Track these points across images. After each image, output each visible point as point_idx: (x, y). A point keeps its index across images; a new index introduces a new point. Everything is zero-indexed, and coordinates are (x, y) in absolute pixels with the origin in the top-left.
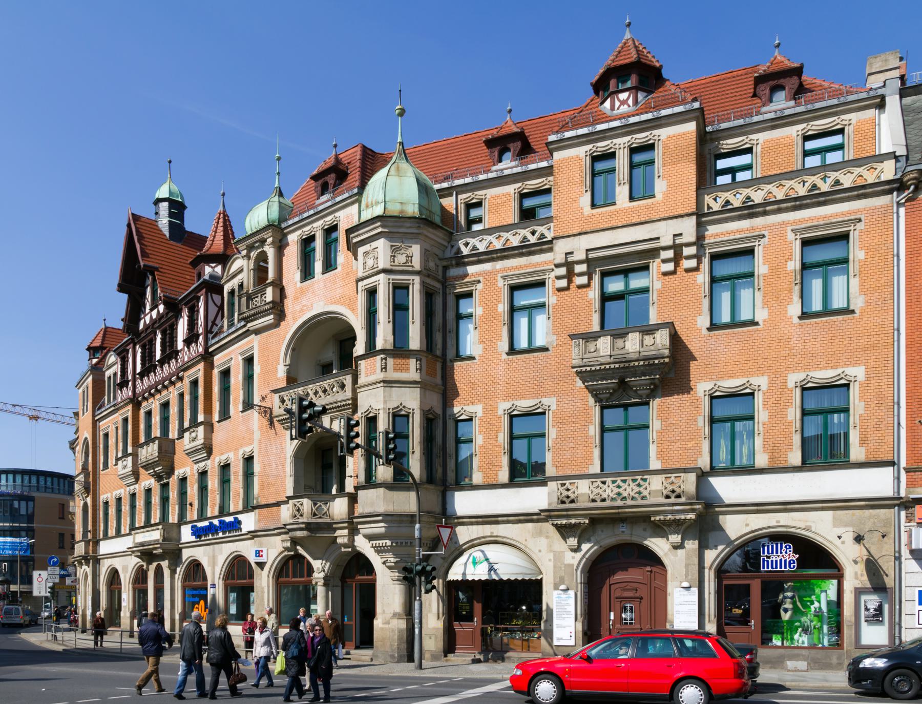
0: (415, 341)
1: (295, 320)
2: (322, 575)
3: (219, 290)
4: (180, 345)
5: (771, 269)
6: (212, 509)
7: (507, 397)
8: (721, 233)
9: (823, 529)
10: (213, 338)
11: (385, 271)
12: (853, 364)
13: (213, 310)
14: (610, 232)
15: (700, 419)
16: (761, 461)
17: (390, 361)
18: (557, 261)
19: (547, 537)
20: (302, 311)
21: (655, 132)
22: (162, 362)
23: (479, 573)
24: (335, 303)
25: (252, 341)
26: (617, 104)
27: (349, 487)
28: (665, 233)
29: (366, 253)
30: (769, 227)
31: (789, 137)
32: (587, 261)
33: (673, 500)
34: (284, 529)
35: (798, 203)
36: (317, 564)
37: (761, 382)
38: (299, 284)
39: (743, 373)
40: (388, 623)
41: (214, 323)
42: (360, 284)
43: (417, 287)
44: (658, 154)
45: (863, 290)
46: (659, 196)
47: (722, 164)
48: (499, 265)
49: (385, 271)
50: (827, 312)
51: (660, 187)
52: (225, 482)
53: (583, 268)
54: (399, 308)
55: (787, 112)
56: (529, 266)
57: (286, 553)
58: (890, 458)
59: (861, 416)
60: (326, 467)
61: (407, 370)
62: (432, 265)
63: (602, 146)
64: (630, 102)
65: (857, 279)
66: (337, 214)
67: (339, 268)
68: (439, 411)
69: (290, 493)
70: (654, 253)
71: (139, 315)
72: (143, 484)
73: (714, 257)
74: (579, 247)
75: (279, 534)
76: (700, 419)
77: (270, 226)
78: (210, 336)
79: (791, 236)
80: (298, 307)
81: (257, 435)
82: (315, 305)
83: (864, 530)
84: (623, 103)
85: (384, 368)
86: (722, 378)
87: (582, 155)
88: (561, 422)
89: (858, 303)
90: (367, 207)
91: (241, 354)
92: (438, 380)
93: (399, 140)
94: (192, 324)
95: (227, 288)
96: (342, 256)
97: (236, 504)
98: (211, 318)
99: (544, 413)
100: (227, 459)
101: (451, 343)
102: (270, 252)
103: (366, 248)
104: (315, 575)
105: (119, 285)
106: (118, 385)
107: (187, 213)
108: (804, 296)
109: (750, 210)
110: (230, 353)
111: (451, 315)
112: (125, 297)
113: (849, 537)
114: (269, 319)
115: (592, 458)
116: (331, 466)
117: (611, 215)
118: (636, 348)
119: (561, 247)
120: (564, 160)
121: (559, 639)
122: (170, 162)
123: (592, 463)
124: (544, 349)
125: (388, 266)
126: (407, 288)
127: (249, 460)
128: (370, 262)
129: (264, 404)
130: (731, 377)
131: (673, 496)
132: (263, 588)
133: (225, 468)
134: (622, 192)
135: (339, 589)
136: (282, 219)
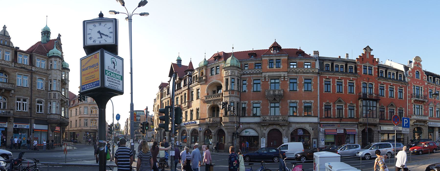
3: (191, 76)
4: (182, 86)
6: (189, 119)
9: (308, 127)
13: (189, 80)
16: (298, 115)
22: (177, 90)
23: (247, 134)
28: (282, 74)
34: (207, 124)
36: (212, 131)
44: (281, 61)
47: (291, 64)
51: (281, 66)
52: (192, 114)
60: (214, 111)
63: (271, 58)
85: (229, 94)
89: (313, 90)
94: (185, 83)
95: (193, 76)
97: (194, 117)
111: (242, 84)
113: (311, 129)
114: (204, 82)
119: (263, 74)
124: (259, 91)
127: (198, 110)
133: (192, 111)
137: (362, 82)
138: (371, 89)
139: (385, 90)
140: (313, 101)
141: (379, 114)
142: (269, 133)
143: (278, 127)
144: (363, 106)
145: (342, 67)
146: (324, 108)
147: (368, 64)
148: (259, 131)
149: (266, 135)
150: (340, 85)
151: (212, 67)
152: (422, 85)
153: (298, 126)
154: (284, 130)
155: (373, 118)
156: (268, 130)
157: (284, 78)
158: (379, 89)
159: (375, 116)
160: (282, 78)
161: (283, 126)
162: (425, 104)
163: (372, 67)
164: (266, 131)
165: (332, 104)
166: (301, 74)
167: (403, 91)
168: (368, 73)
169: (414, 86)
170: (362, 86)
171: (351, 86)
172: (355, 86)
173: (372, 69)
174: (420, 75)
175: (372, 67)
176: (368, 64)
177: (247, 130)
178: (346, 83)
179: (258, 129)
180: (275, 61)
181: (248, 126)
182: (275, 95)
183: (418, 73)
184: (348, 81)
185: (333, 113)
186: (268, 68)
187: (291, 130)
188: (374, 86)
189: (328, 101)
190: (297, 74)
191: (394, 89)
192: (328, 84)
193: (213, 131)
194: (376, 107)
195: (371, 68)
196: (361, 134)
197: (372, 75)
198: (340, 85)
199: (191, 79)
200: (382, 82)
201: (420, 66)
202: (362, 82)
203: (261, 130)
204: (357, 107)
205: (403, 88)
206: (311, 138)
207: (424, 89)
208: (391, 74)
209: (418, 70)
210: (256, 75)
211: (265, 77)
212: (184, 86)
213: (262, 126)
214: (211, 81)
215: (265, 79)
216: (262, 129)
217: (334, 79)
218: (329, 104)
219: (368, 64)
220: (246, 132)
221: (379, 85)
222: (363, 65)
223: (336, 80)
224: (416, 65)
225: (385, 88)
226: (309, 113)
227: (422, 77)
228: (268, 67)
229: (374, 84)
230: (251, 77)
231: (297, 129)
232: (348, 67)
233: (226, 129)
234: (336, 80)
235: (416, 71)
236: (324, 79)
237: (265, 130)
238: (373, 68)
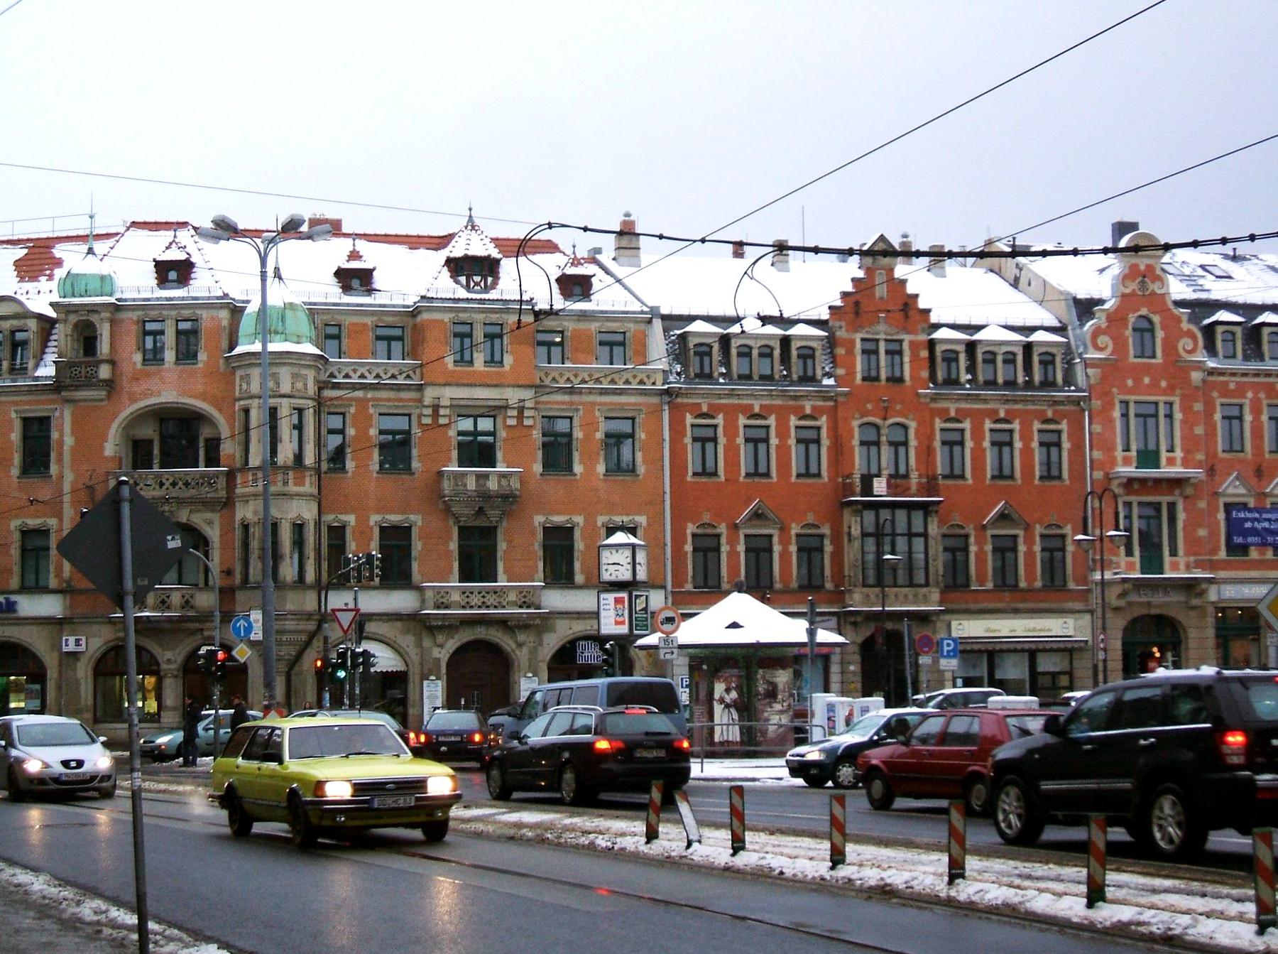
1: (133, 400)
7: (378, 511)
12: (639, 514)
24: (194, 397)
27: (216, 578)
28: (513, 396)
29: (242, 378)
32: (451, 406)
42: (237, 404)
46: (507, 367)
51: (508, 360)
67: (200, 365)
70: (506, 407)
82: (164, 393)
87: (446, 320)
88: (425, 536)
89: (641, 469)
115: (452, 568)
117: (469, 373)
119: (430, 394)
137: (855, 423)
138: (902, 450)
139: (969, 444)
140: (642, 520)
141: (939, 561)
144: (864, 535)
146: (689, 548)
147: (882, 331)
148: (413, 652)
149: (444, 670)
150: (757, 441)
152: (1170, 390)
153: (579, 627)
154: (520, 645)
155: (911, 585)
156: (452, 645)
157: (520, 416)
158: (937, 444)
159: (920, 578)
160: (510, 413)
162: (1189, 491)
163: (901, 341)
164: (443, 650)
165: (722, 529)
166: (591, 398)
167: (1064, 436)
168: (883, 376)
169: (1126, 403)
170: (856, 442)
171: (809, 441)
172: (825, 442)
173: (900, 353)
174: (1160, 334)
175: (901, 341)
176: (882, 327)
178: (783, 433)
179: (407, 641)
180: (479, 335)
182: (486, 496)
183: (1145, 330)
184: (793, 421)
186: (451, 366)
187: (552, 642)
188: (912, 433)
189: (706, 518)
190: (576, 398)
191: (1016, 436)
192: (705, 440)
194: (925, 535)
195: (895, 347)
196: (857, 658)
197: (900, 380)
198: (757, 441)
200: (953, 409)
201: (1155, 287)
202: (855, 423)
204: (837, 538)
205: (1064, 426)
207: (1186, 409)
208: (1000, 359)
209: (1144, 311)
210: (392, 394)
211: (436, 408)
214: (147, 394)
215: (435, 415)
216: (427, 642)
218: (709, 531)
219: (882, 331)
221: (938, 424)
222: (858, 337)
223: (742, 421)
224: (1132, 287)
225: (968, 435)
227: (1170, 347)
228: (449, 360)
229: (912, 425)
232: (794, 353)
234: (742, 421)
235: (1132, 318)
236: (689, 420)
237: (441, 646)
238: (906, 346)
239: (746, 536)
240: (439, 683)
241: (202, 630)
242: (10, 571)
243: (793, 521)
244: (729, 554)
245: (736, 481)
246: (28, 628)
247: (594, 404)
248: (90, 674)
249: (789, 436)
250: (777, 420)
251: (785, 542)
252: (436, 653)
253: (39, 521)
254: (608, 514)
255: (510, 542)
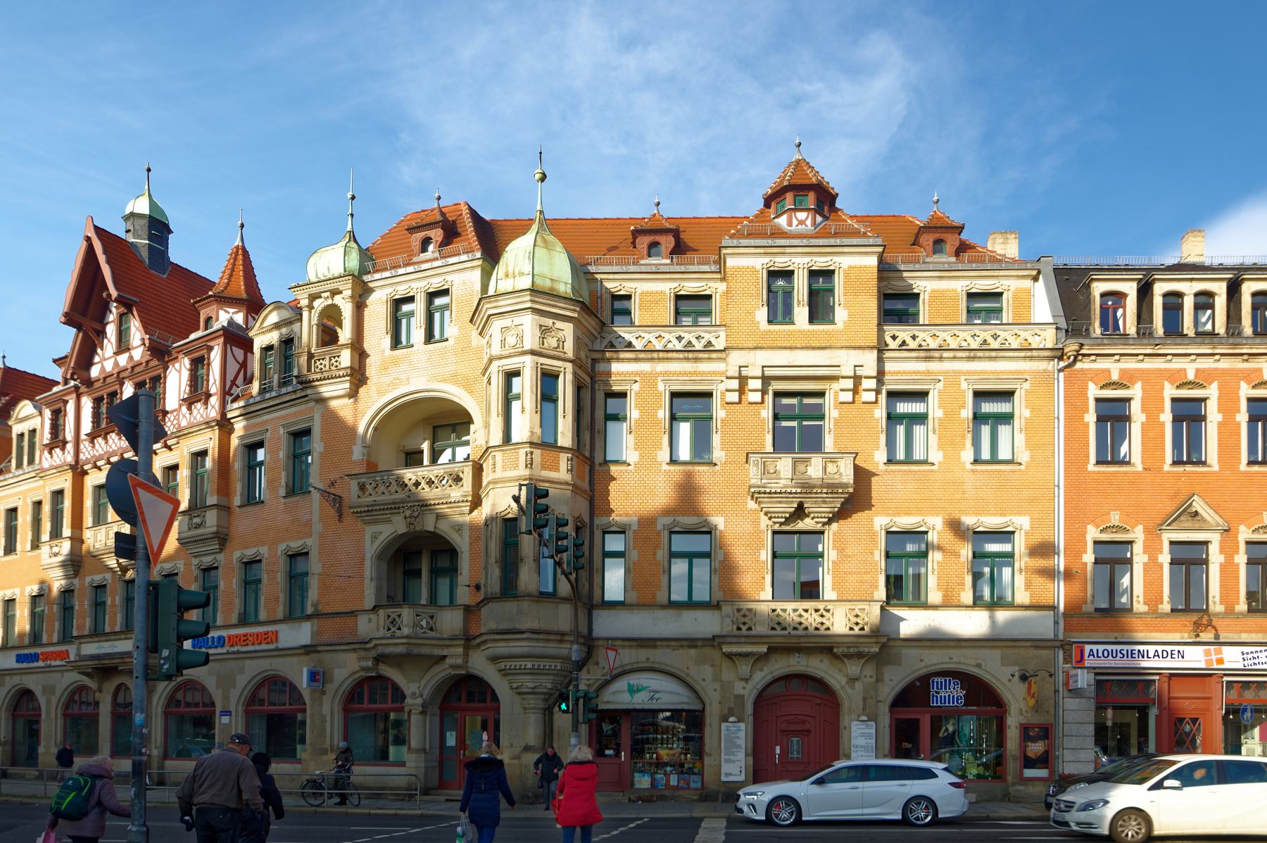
0: (565, 436)
1: (381, 393)
2: (419, 701)
5: (945, 414)
8: (902, 371)
10: (233, 401)
11: (533, 353)
12: (1019, 513)
13: (233, 368)
14: (788, 352)
15: (877, 554)
17: (537, 452)
18: (729, 374)
19: (712, 666)
20: (393, 385)
21: (836, 259)
23: (640, 701)
24: (445, 381)
25: (312, 409)
26: (795, 222)
27: (464, 595)
28: (847, 361)
29: (505, 329)
30: (945, 373)
31: (955, 291)
33: (779, 632)
35: (972, 354)
37: (264, 550)
38: (388, 352)
39: (920, 511)
40: (518, 757)
41: (233, 383)
43: (569, 377)
44: (839, 281)
45: (1029, 446)
48: (661, 367)
49: (533, 353)
50: (994, 460)
51: (841, 314)
53: (757, 384)
54: (547, 395)
55: (662, 269)
56: (695, 373)
57: (363, 674)
58: (1050, 602)
59: (834, 562)
61: (557, 469)
62: (583, 355)
64: (809, 222)
65: (1023, 435)
66: (449, 278)
68: (587, 520)
69: (369, 602)
71: (92, 357)
72: (88, 579)
73: (892, 395)
74: (755, 362)
75: (354, 650)
76: (877, 554)
77: (347, 274)
78: (229, 399)
79: (964, 385)
80: (387, 380)
81: (317, 527)
83: (1031, 668)
84: (801, 222)
85: (530, 465)
86: (898, 514)
87: (759, 267)
89: (1023, 456)
90: (507, 276)
91: (284, 426)
92: (586, 486)
93: (539, 208)
96: (453, 326)
98: (230, 377)
99: (1013, 533)
100: (258, 553)
101: (598, 445)
102: (347, 309)
103: (506, 322)
104: (409, 701)
105: (66, 315)
106: (46, 445)
107: (172, 238)
108: (976, 443)
109: (927, 354)
110: (263, 423)
111: (599, 414)
112: (72, 331)
115: (763, 584)
116: (418, 573)
117: (790, 333)
118: (820, 474)
120: (739, 269)
121: (727, 775)
122: (149, 170)
123: (763, 590)
125: (536, 347)
126: (557, 377)
127: (10, 548)
128: (511, 340)
129: (332, 490)
130: (907, 514)
131: (778, 628)
132: (324, 716)
134: (801, 312)
135: (437, 719)
136: (363, 271)
142: (761, 700)
143: (817, 666)
145: (1204, 301)
149: (749, 708)
151: (401, 291)
154: (852, 680)
156: (762, 677)
161: (850, 656)
164: (749, 683)
165: (1138, 534)
177: (635, 679)
181: (642, 655)
185: (1147, 584)
187: (895, 680)
189: (1115, 518)
193: (416, 688)
199: (244, 365)
203: (717, 678)
206: (1013, 723)
211: (743, 380)
212: (189, 402)
213: (729, 656)
217: (1152, 381)
220: (633, 690)
226: (1234, 695)
230: (654, 375)
231: (925, 680)
233: (504, 673)
237: (746, 680)
239: (1172, 543)
240: (742, 725)
241: (445, 657)
242: (277, 599)
243: (1242, 522)
244: (1146, 567)
245: (1160, 469)
246: (289, 659)
247: (958, 373)
248: (337, 709)
249: (1239, 411)
250: (1220, 388)
251: (1228, 549)
252: (739, 688)
253: (300, 543)
254: (977, 514)
255: (841, 550)
